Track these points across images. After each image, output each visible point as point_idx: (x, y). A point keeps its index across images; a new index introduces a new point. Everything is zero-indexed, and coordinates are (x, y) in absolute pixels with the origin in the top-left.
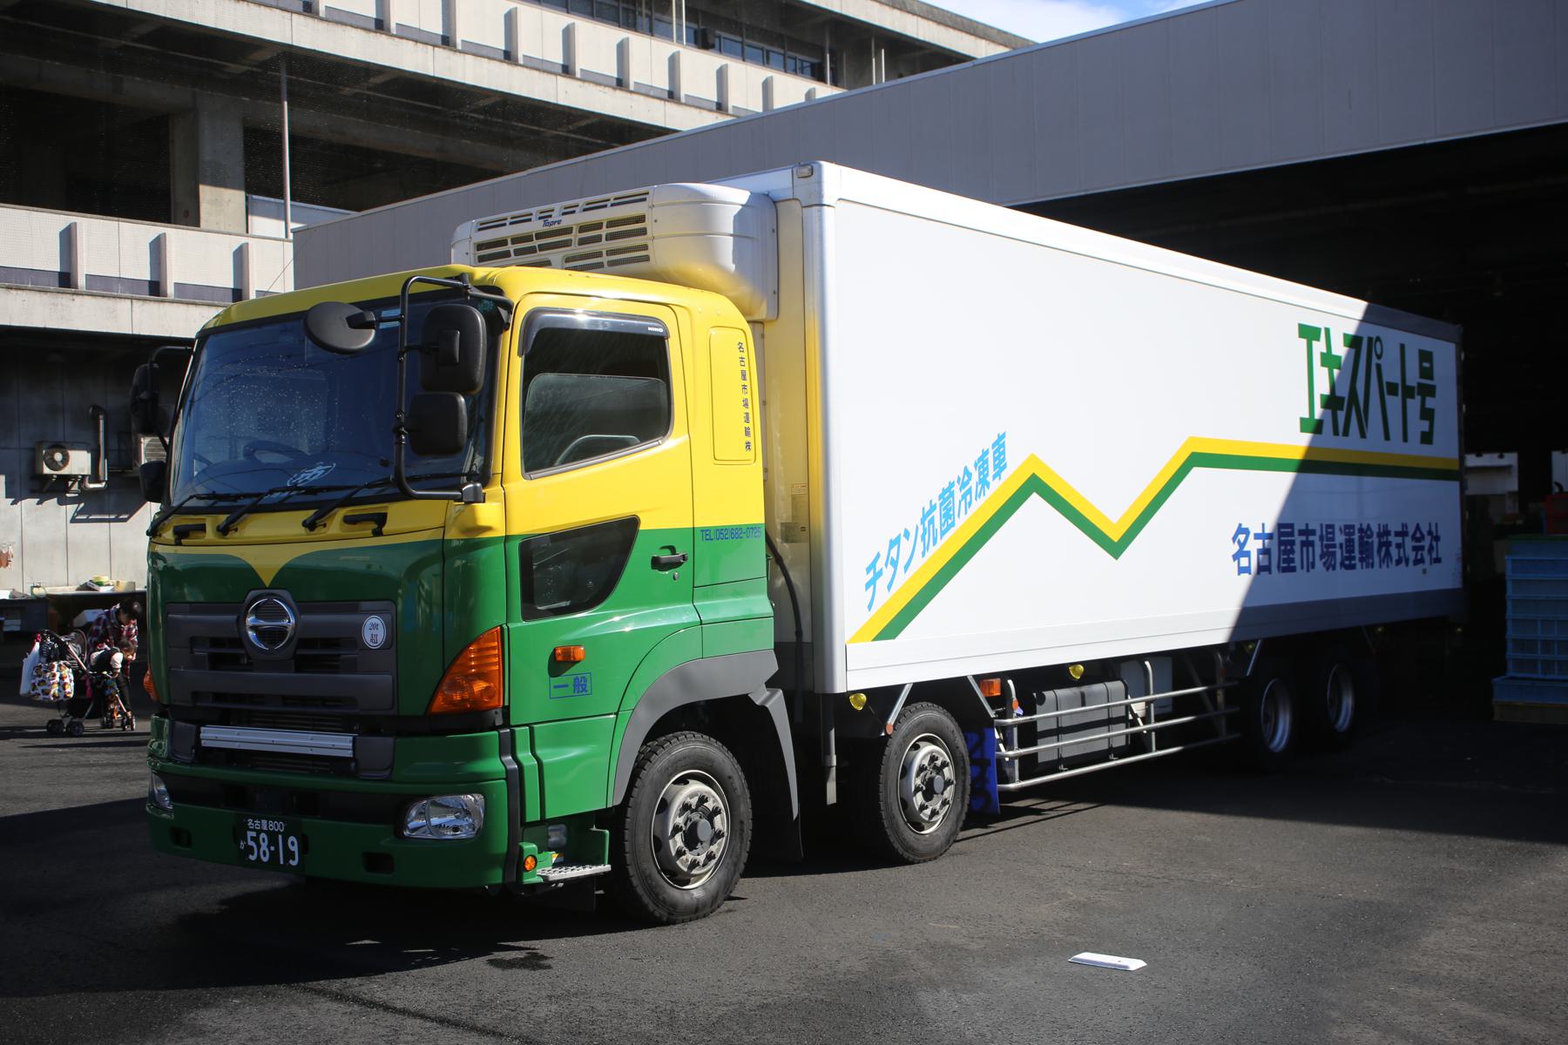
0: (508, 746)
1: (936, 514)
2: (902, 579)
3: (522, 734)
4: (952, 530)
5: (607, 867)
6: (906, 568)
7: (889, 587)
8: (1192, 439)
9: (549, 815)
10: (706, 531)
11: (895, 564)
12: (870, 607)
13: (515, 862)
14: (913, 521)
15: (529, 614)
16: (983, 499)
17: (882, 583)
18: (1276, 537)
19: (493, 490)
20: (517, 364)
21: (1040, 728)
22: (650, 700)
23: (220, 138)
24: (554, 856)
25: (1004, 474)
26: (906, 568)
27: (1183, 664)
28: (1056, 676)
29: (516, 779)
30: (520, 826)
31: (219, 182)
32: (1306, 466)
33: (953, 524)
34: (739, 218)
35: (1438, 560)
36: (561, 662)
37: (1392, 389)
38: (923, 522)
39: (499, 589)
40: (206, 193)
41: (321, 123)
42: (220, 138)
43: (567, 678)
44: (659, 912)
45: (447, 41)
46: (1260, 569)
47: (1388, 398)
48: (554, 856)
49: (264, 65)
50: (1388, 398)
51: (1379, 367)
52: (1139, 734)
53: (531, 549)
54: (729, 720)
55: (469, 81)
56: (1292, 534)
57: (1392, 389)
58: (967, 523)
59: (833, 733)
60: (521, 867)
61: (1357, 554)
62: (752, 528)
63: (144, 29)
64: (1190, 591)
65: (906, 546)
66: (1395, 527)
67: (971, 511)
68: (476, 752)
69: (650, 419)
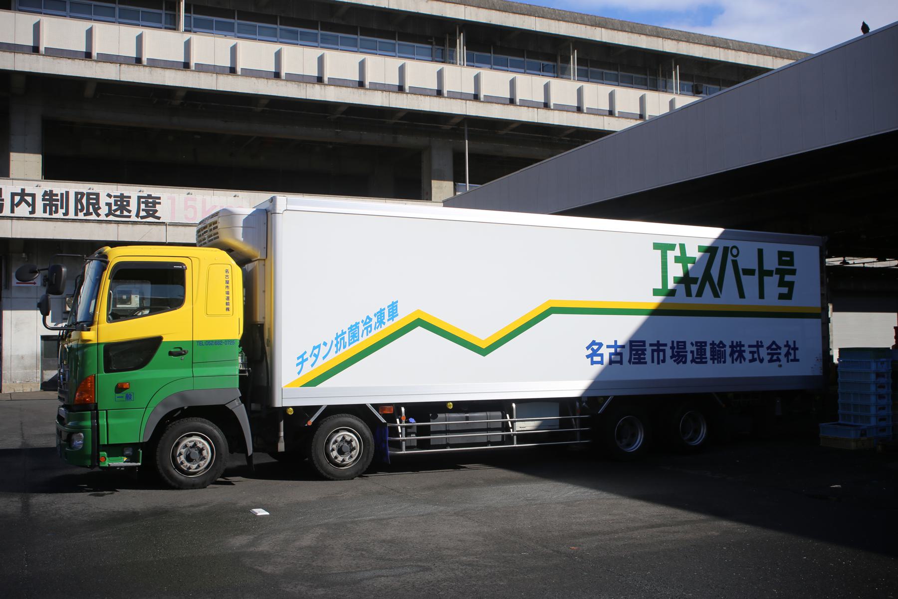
0: (96, 417)
1: (346, 336)
2: (320, 362)
3: (102, 414)
4: (357, 343)
5: (139, 464)
6: (324, 358)
7: (312, 365)
8: (550, 301)
9: (110, 442)
10: (200, 343)
11: (317, 356)
12: (299, 373)
13: (96, 459)
14: (330, 338)
15: (107, 370)
16: (377, 331)
17: (307, 365)
18: (628, 348)
19: (94, 327)
20: (108, 281)
21: (432, 429)
22: (164, 403)
23: (441, 158)
24: (125, 459)
25: (396, 319)
26: (324, 358)
27: (564, 405)
28: (439, 408)
29: (96, 429)
30: (98, 447)
31: (441, 178)
32: (656, 312)
33: (358, 340)
34: (246, 220)
35: (795, 360)
36: (120, 389)
37: (749, 272)
38: (336, 339)
39: (95, 363)
40: (435, 183)
41: (486, 147)
42: (441, 158)
43: (123, 394)
44: (173, 484)
45: (546, 105)
46: (611, 362)
47: (745, 279)
48: (125, 459)
49: (459, 124)
50: (745, 279)
51: (735, 263)
52: (510, 435)
53: (110, 348)
54: (219, 415)
55: (556, 123)
56: (644, 345)
57: (749, 272)
58: (365, 340)
59: (282, 423)
60: (99, 461)
61: (708, 354)
62: (231, 342)
63: (401, 114)
64: (559, 370)
65: (324, 350)
66: (717, 342)
67: (370, 335)
68: (83, 418)
69: (177, 302)
